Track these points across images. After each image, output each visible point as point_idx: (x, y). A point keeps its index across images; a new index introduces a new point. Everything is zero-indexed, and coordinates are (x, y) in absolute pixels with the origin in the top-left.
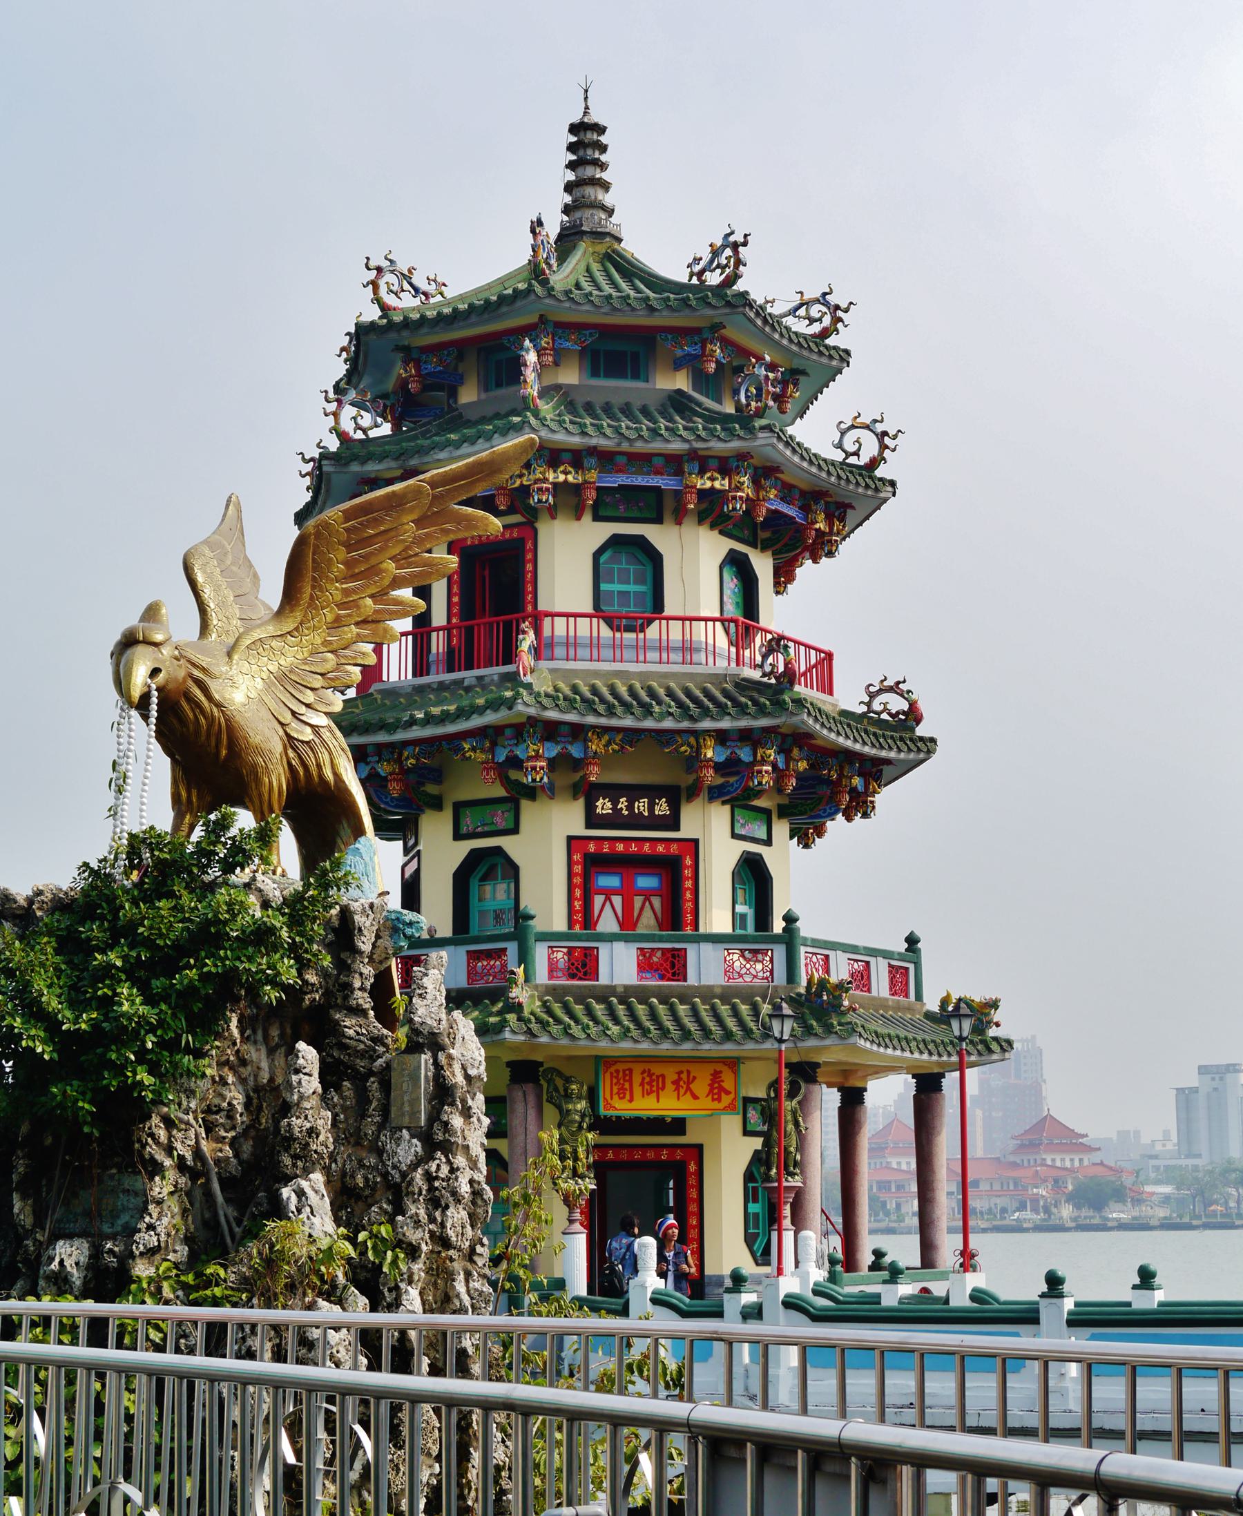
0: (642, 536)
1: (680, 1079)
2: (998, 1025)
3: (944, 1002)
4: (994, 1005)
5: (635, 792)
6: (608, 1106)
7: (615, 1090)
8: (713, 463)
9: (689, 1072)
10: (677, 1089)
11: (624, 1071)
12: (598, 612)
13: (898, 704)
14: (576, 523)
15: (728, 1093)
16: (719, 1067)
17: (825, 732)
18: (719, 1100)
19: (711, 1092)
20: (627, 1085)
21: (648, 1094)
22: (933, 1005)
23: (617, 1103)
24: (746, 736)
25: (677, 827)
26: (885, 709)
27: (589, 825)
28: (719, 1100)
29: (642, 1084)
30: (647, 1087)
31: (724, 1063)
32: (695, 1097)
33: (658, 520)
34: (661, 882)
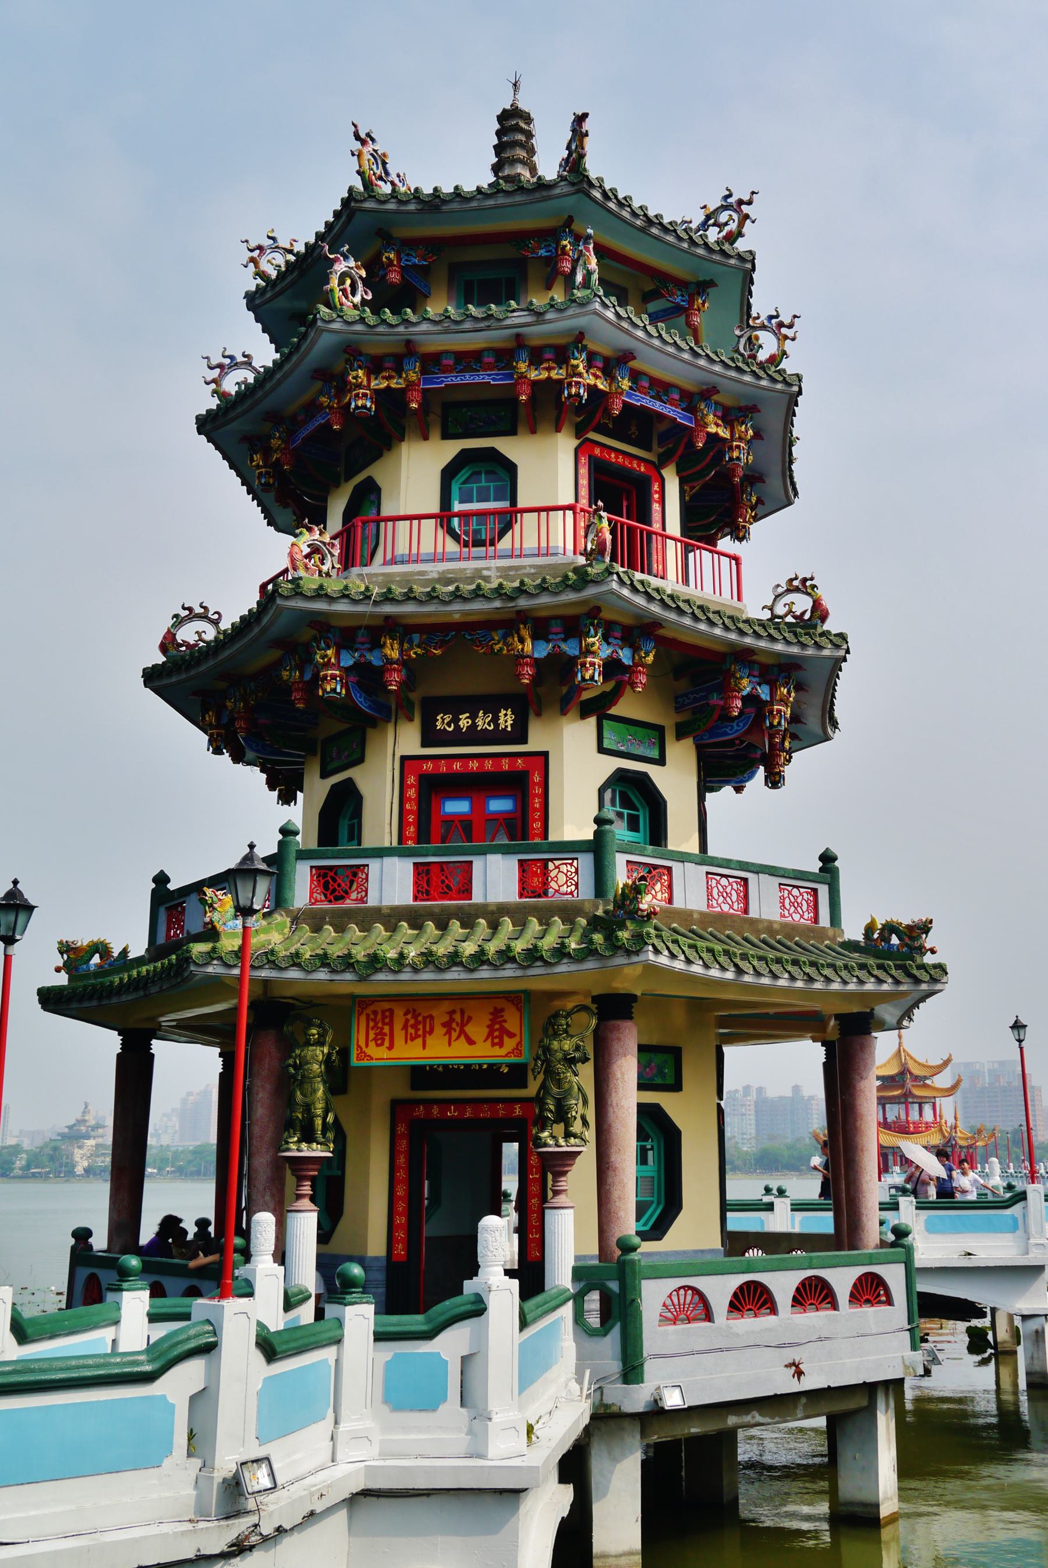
0: (493, 448)
1: (452, 1020)
2: (933, 951)
3: (869, 929)
4: (925, 927)
5: (472, 704)
6: (362, 1055)
7: (372, 1036)
8: (549, 354)
9: (462, 1012)
10: (449, 1033)
11: (383, 1012)
12: (444, 517)
13: (802, 604)
14: (426, 442)
15: (511, 1035)
16: (500, 1003)
17: (672, 616)
18: (501, 1045)
19: (490, 1035)
20: (386, 1029)
21: (412, 1039)
22: (853, 930)
23: (372, 1050)
24: (573, 625)
25: (524, 741)
26: (790, 611)
27: (424, 744)
28: (501, 1045)
29: (405, 1027)
30: (411, 1031)
31: (506, 998)
32: (471, 1042)
33: (512, 432)
34: (515, 805)
